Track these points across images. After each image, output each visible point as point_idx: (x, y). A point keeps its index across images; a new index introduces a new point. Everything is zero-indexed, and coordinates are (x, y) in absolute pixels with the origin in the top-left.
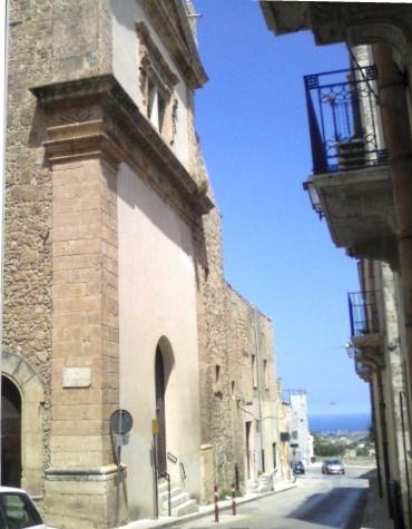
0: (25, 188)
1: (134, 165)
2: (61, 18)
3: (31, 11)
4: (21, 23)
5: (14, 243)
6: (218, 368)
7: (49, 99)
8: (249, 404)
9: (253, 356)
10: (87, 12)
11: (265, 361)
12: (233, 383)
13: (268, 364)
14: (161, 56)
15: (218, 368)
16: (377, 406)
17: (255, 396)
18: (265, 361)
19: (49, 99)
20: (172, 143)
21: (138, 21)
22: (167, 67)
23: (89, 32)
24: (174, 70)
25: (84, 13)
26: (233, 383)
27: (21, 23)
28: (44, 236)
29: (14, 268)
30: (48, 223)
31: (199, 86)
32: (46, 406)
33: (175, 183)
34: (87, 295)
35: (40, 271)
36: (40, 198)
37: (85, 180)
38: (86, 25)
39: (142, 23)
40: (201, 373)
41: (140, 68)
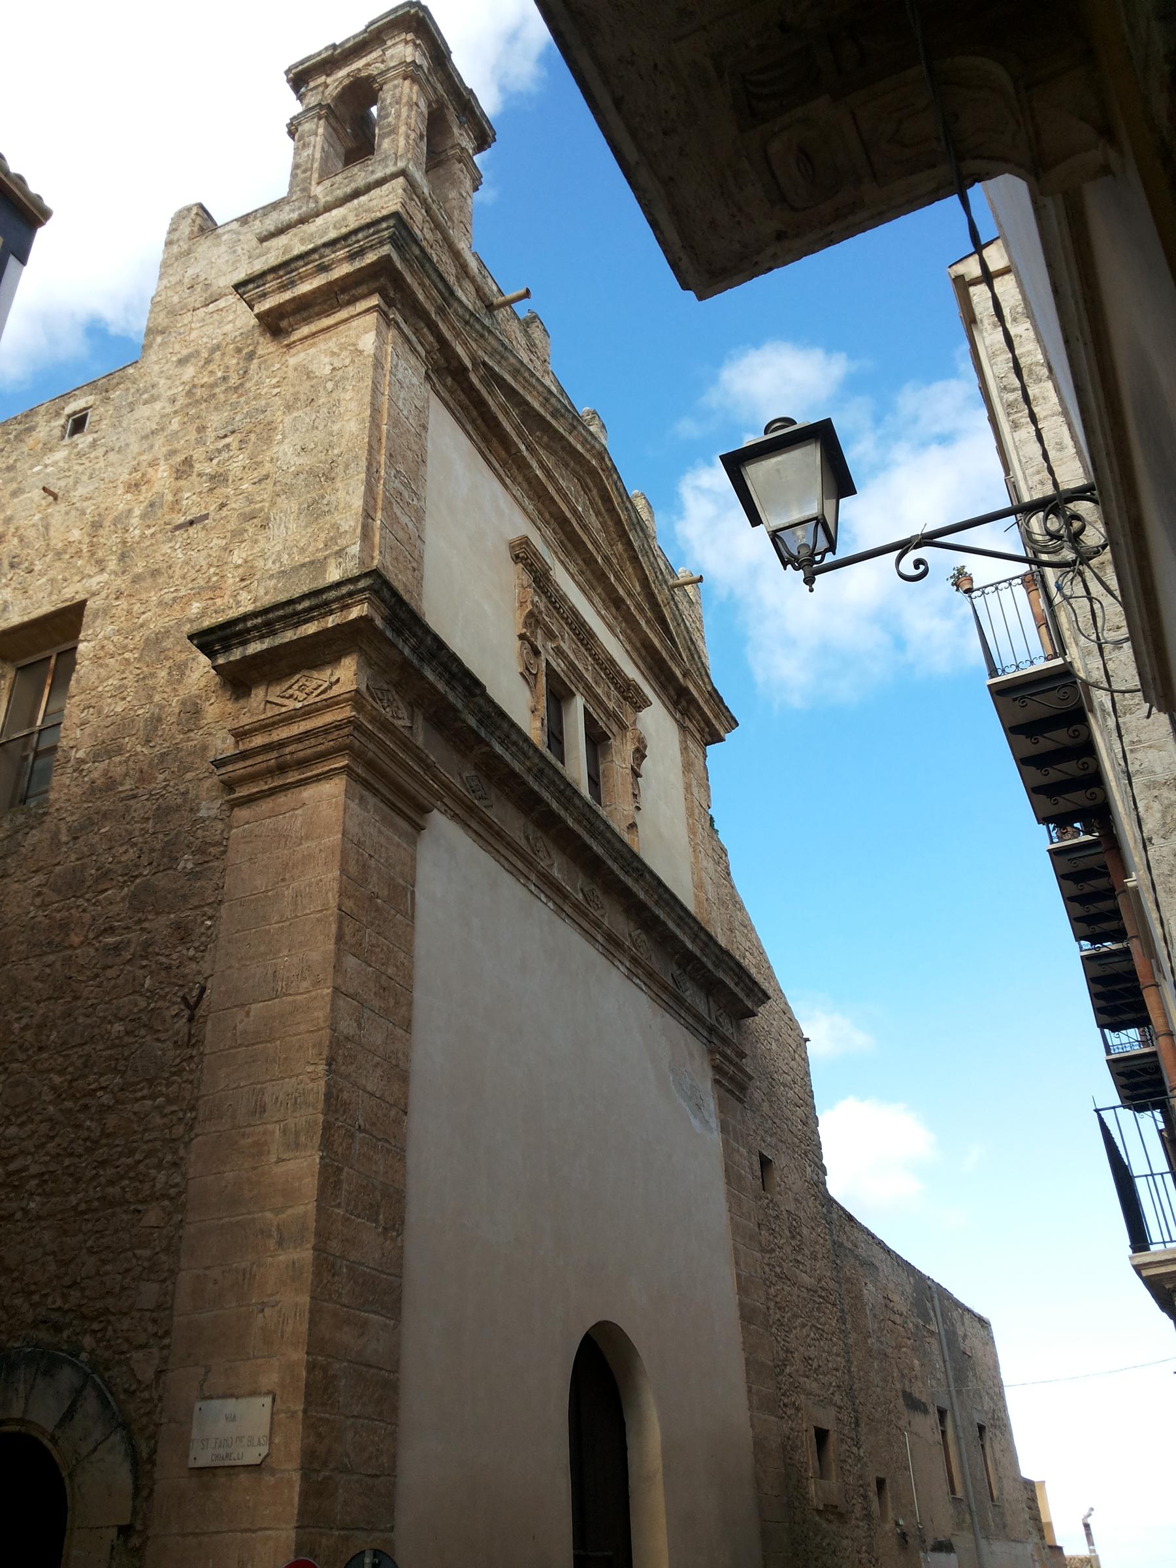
0: (162, 881)
1: (470, 817)
2: (288, 490)
3: (230, 491)
4: (206, 516)
5: (118, 1027)
6: (821, 1436)
7: (236, 654)
8: (944, 1547)
9: (942, 1413)
10: (347, 466)
11: (981, 1429)
12: (881, 1483)
13: (988, 1434)
14: (591, 635)
15: (821, 1436)
16: (614, 495)
17: (959, 1525)
18: (981, 1429)
19: (236, 654)
20: (633, 826)
21: (513, 535)
22: (612, 662)
23: (348, 506)
24: (631, 671)
25: (340, 470)
26: (881, 1483)
27: (206, 516)
28: (192, 1001)
29: (106, 1099)
30: (206, 967)
31: (717, 738)
32: (135, 1541)
33: (665, 941)
34: (280, 1160)
35: (169, 1101)
36: (195, 901)
37: (307, 837)
38: (341, 494)
39: (525, 542)
40: (759, 1445)
41: (522, 637)
